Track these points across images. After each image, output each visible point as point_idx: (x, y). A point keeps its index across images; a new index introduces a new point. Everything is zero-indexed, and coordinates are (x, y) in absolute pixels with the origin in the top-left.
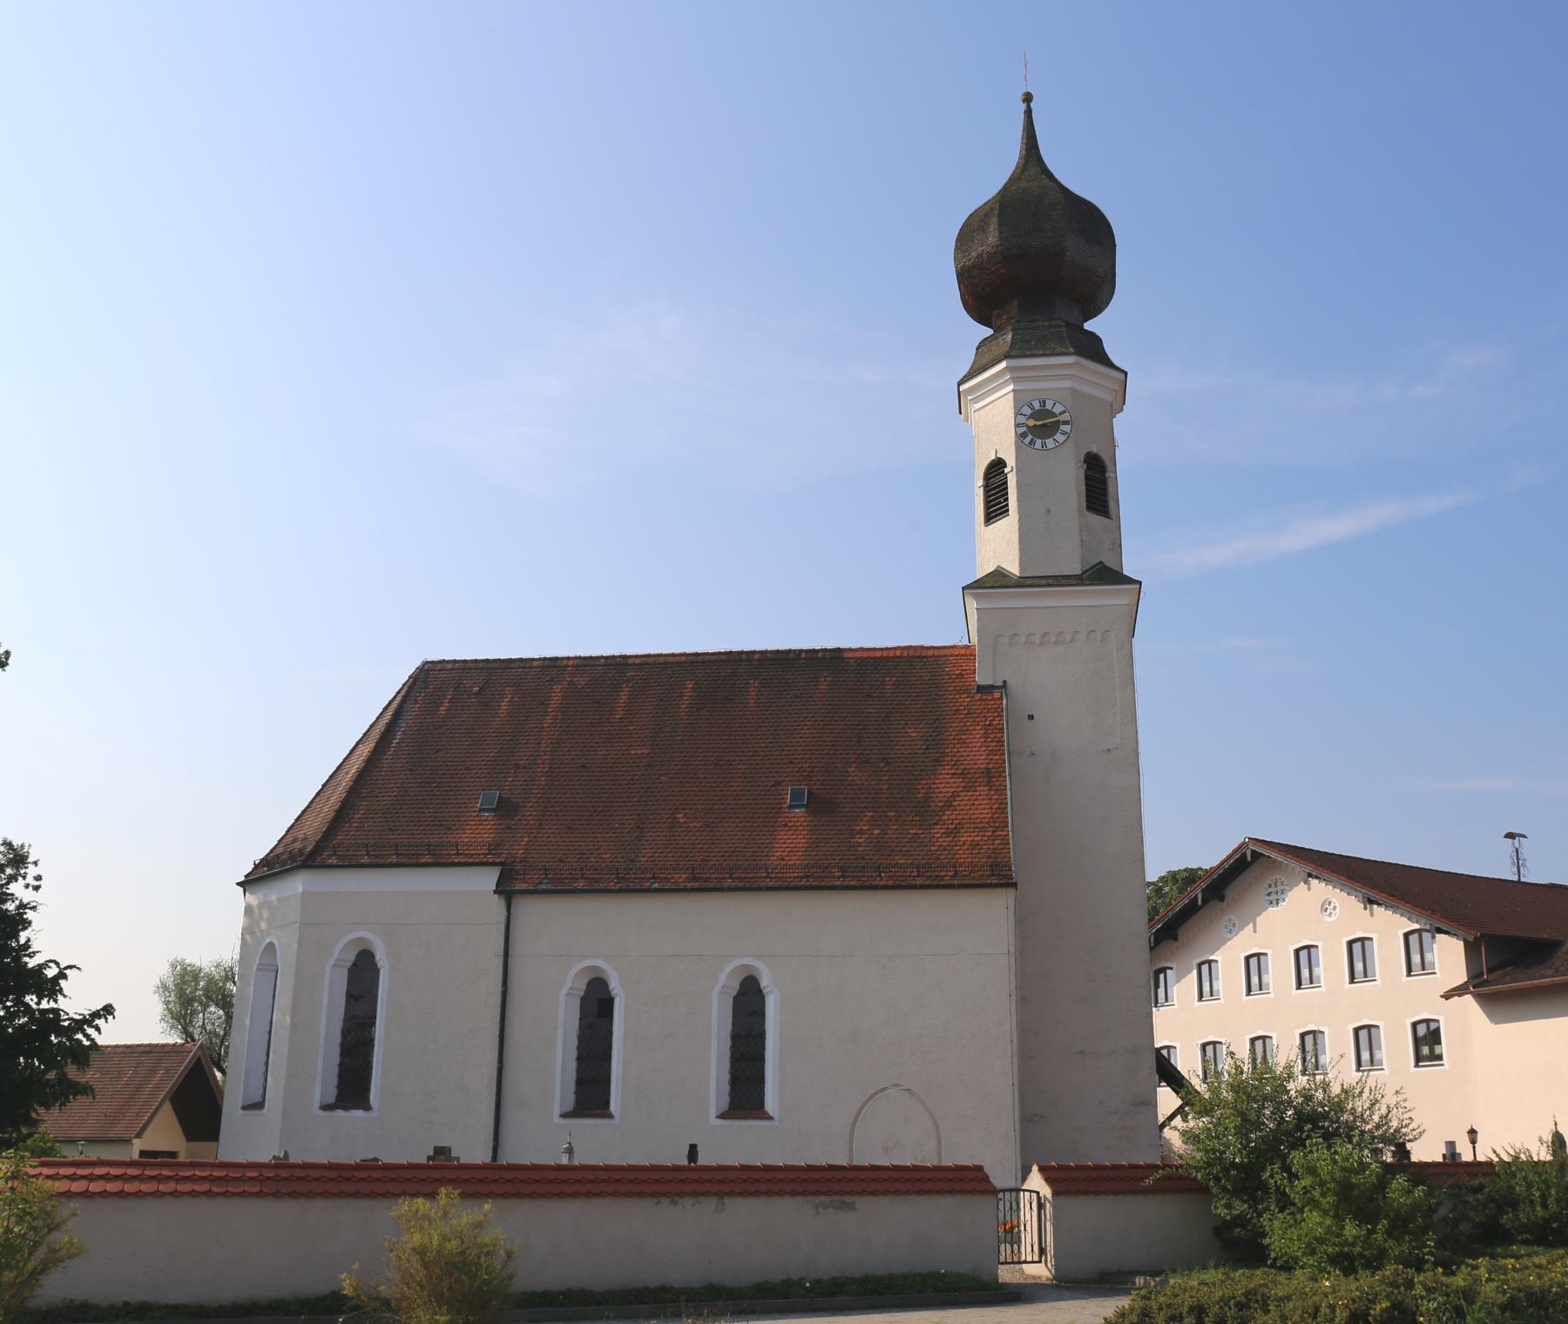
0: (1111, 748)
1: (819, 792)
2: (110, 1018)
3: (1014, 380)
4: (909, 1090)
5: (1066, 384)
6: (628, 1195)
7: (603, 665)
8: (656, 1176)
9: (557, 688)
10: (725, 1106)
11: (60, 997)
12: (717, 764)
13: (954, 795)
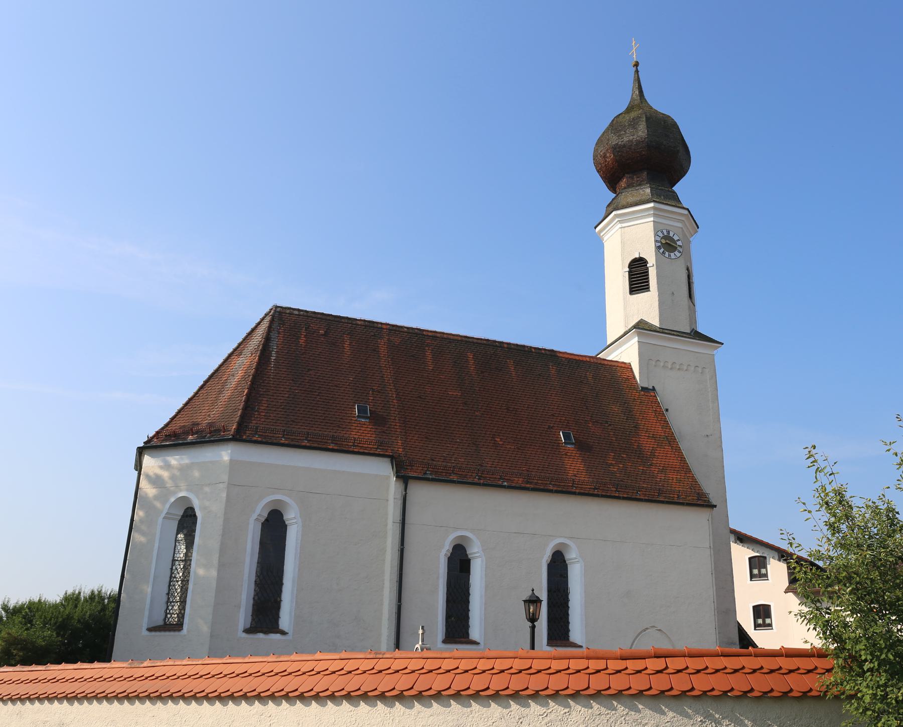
3: (655, 215)
4: (660, 630)
10: (248, 626)
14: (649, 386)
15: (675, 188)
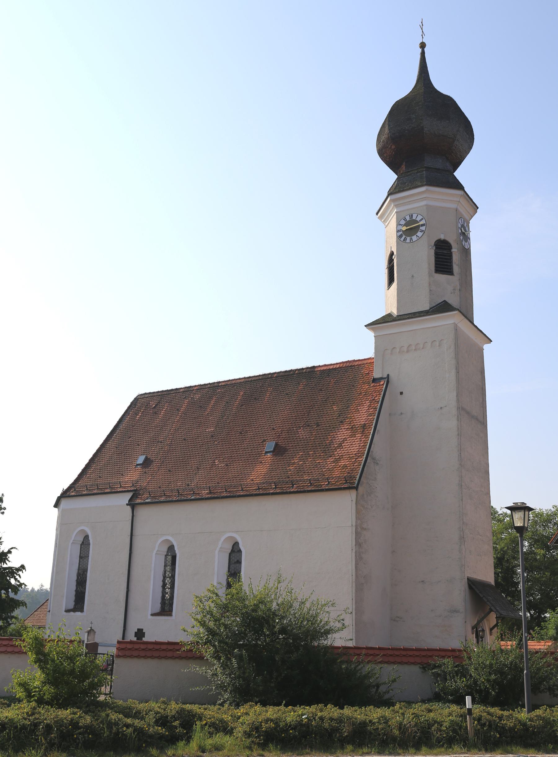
0: (442, 406)
1: (285, 445)
2: (24, 571)
3: (396, 206)
5: (424, 203)
6: (131, 657)
7: (209, 388)
8: (157, 647)
9: (186, 401)
11: (7, 562)
12: (241, 433)
13: (345, 440)
14: (382, 375)
15: (396, 177)
